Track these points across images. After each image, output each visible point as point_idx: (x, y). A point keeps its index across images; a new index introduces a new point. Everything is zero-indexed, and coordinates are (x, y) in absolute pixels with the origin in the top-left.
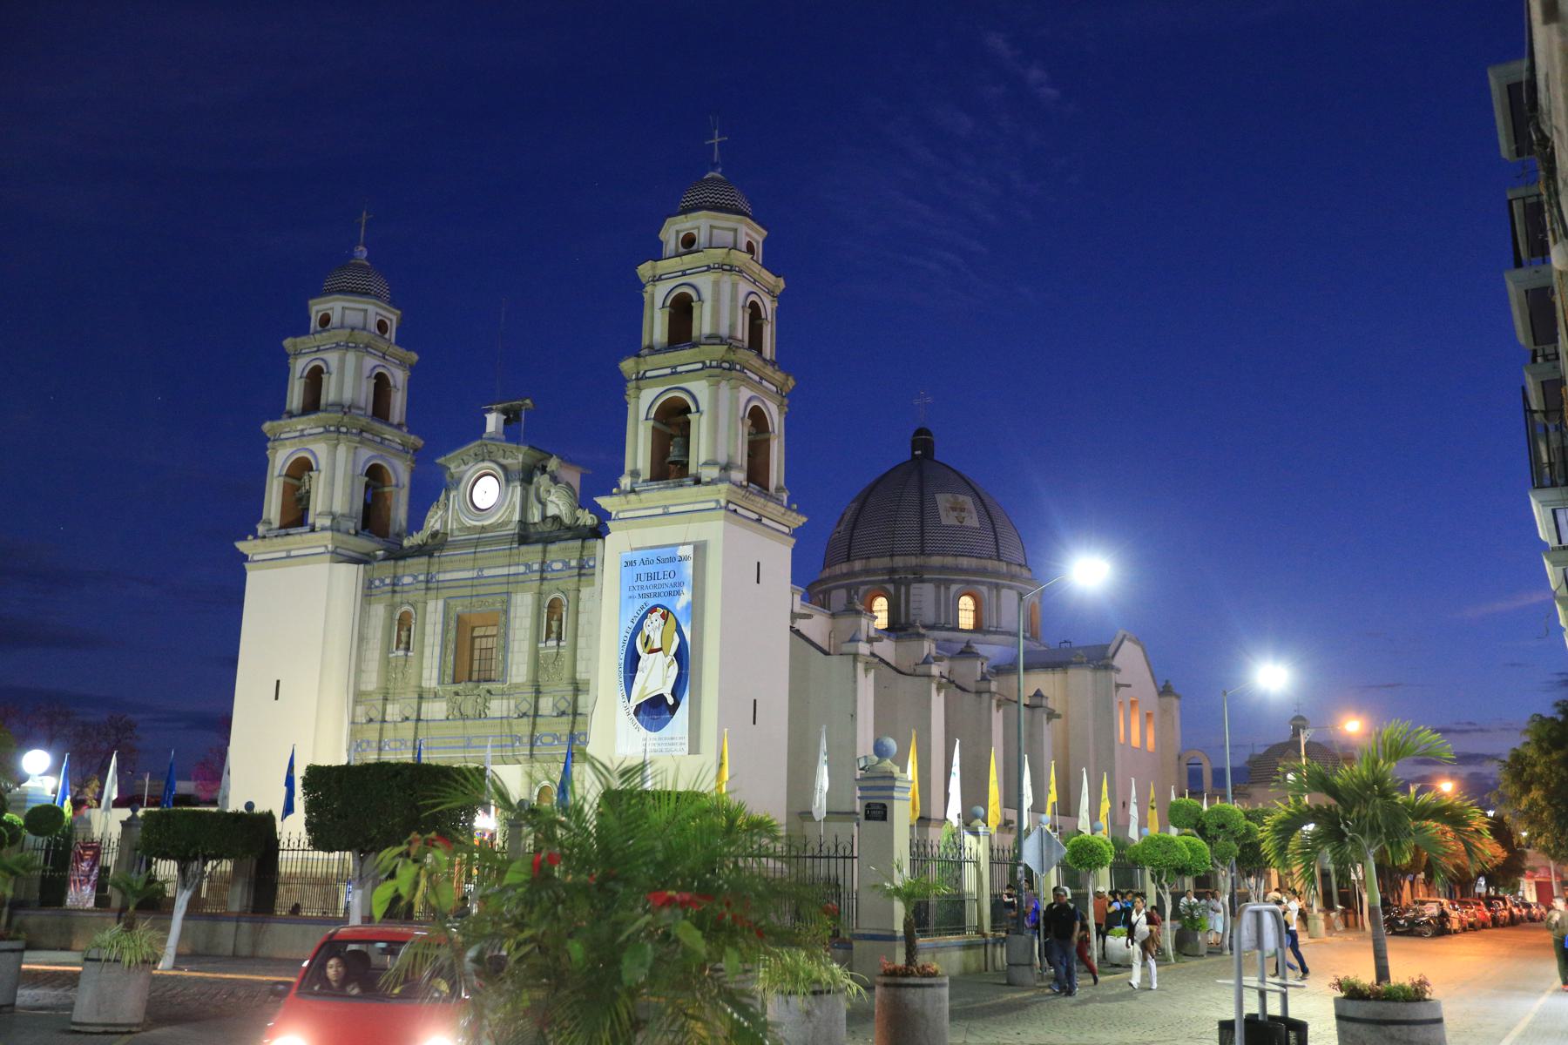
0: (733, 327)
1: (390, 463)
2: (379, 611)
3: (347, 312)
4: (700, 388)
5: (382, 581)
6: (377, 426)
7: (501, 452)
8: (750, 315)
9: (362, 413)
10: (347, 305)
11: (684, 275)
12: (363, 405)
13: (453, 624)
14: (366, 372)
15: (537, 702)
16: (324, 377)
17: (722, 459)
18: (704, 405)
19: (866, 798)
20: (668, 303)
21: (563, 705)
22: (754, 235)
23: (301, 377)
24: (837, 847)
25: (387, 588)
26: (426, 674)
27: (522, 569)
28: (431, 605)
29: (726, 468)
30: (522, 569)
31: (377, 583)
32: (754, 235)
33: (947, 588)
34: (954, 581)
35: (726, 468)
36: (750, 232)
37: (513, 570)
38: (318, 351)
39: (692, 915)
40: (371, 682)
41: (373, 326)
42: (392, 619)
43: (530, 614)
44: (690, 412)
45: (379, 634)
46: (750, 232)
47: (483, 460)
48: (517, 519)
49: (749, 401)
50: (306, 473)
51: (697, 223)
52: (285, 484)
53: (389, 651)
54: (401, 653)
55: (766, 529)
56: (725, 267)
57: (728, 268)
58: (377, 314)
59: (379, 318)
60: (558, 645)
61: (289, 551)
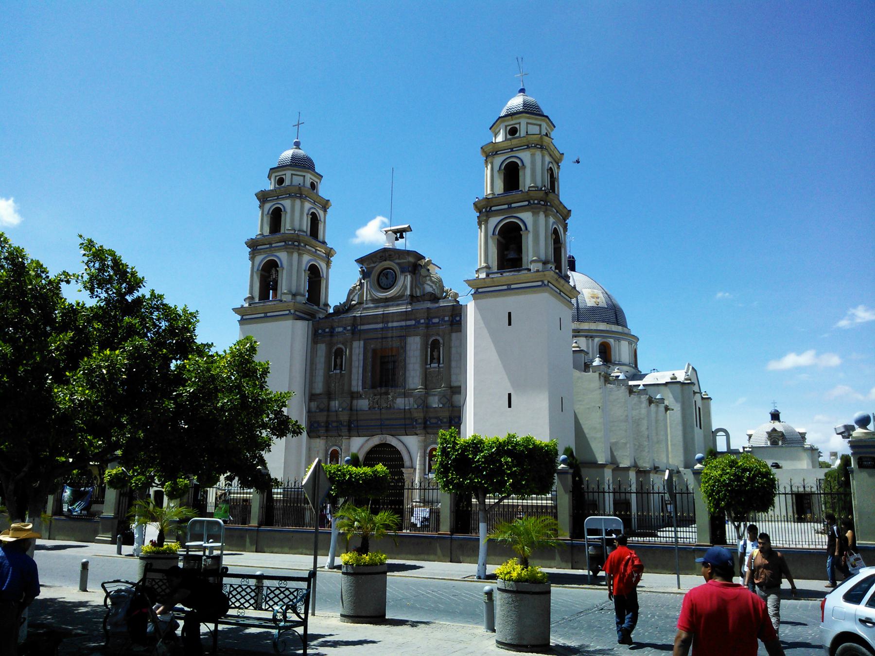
0: (301, 225)
1: (317, 262)
2: (322, 348)
3: (294, 176)
4: (527, 217)
5: (324, 331)
6: (314, 242)
7: (397, 255)
8: (311, 219)
9: (305, 234)
10: (530, 121)
11: (512, 150)
12: (305, 230)
13: (370, 355)
14: (306, 211)
15: (351, 403)
16: (283, 214)
17: (543, 257)
18: (530, 227)
19: (860, 453)
20: (503, 167)
21: (322, 406)
22: (314, 178)
23: (268, 213)
24: (288, 483)
25: (327, 334)
26: (354, 383)
27: (413, 322)
28: (355, 344)
29: (545, 263)
30: (413, 322)
31: (320, 331)
32: (314, 178)
33: (593, 340)
34: (597, 336)
35: (545, 263)
36: (548, 128)
37: (409, 323)
38: (278, 199)
39: (311, 518)
40: (319, 388)
41: (308, 184)
42: (427, 344)
43: (324, 355)
44: (521, 230)
45: (323, 360)
46: (548, 128)
47: (385, 261)
48: (409, 293)
49: (308, 262)
50: (274, 269)
51: (518, 121)
52: (261, 275)
53: (329, 370)
54: (338, 371)
55: (562, 298)
56: (538, 146)
57: (539, 147)
58: (310, 178)
59: (311, 181)
60: (439, 366)
61: (266, 313)
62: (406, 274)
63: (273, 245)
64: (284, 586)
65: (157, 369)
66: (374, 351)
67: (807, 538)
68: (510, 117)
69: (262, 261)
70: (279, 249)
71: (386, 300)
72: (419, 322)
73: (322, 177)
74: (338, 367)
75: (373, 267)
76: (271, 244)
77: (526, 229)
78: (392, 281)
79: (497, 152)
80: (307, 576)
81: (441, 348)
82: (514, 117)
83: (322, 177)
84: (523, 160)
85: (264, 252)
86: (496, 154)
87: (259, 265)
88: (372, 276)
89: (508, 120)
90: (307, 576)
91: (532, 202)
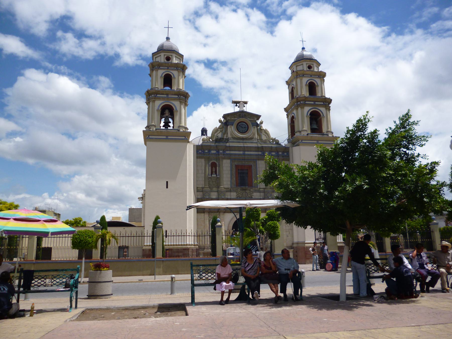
11: (311, 76)
38: (168, 69)
62: (254, 127)
63: (169, 96)
64: (35, 288)
65: (342, 162)
66: (236, 166)
67: (25, 251)
68: (309, 60)
69: (161, 104)
70: (175, 99)
71: (243, 139)
72: (224, 152)
73: (320, 64)
74: (214, 173)
75: (235, 120)
76: (167, 95)
77: (323, 115)
78: (239, 129)
79: (303, 75)
80: (261, 285)
81: (217, 168)
82: (311, 60)
83: (320, 64)
84: (306, 82)
85: (163, 99)
86: (303, 76)
87: (159, 106)
88: (234, 125)
89: (308, 61)
90: (261, 285)
91: (325, 103)
